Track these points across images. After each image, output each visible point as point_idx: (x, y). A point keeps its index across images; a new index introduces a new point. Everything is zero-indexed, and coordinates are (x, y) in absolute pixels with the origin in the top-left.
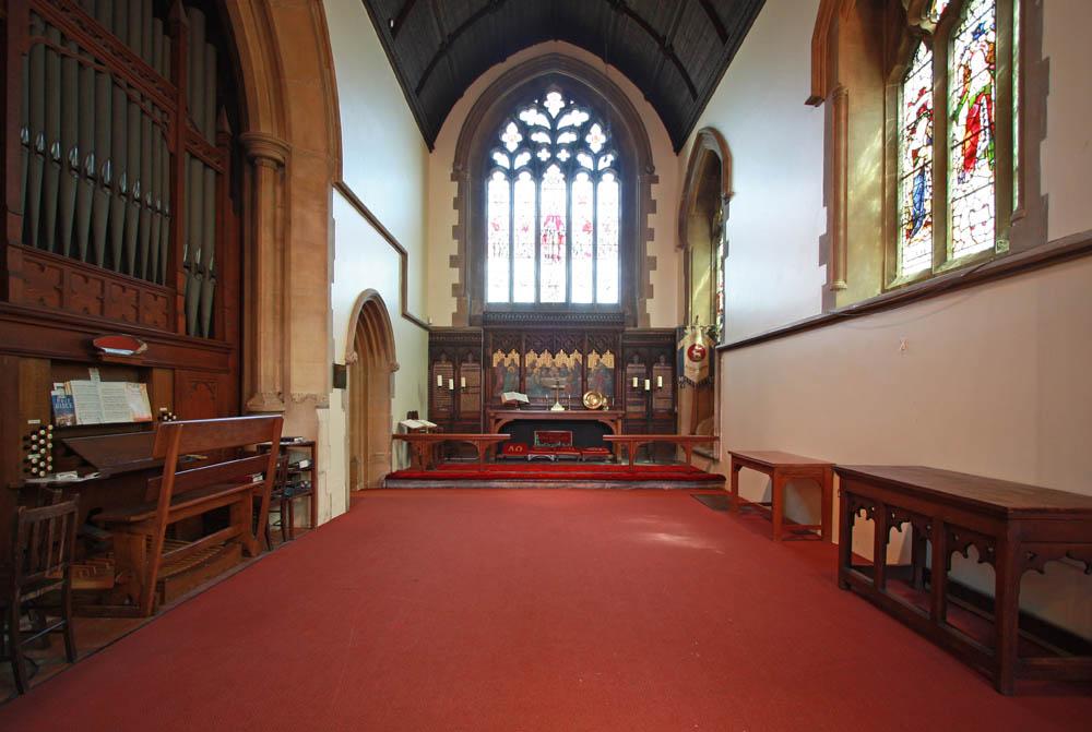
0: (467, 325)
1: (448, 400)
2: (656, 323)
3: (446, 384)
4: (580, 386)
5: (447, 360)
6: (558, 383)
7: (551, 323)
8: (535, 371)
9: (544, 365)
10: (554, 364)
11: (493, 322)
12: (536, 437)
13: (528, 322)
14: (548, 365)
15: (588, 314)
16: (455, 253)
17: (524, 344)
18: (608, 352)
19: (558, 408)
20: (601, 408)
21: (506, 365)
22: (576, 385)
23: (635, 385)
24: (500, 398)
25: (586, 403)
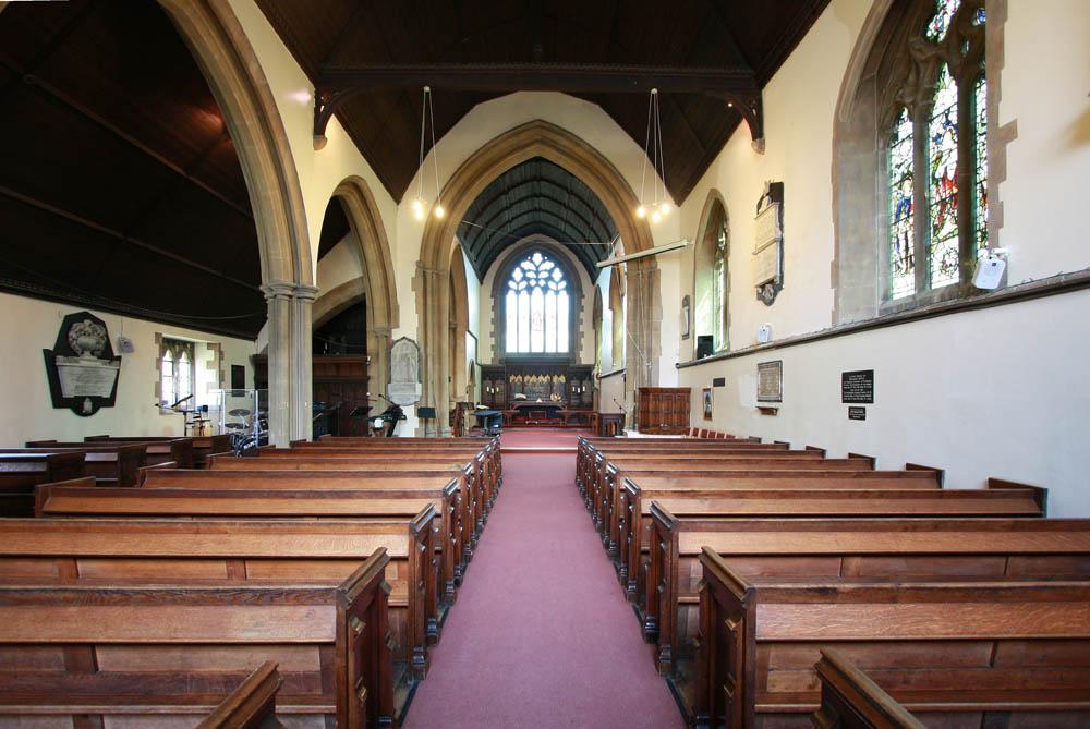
19: (539, 401)
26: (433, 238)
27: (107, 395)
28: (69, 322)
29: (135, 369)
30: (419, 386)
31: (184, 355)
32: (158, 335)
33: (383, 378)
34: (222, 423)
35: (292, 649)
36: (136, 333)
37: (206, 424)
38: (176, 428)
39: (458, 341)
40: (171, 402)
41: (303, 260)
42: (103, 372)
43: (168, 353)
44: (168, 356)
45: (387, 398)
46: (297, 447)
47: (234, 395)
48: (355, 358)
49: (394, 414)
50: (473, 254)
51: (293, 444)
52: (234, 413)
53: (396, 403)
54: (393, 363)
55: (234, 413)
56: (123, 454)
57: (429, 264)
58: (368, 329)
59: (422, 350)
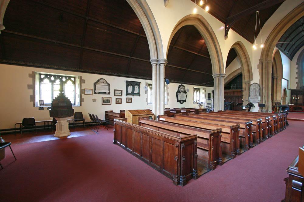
1: (295, 101)
2: (48, 100)
3: (295, 98)
16: (297, 86)
26: (265, 53)
27: (185, 100)
28: (180, 86)
29: (190, 94)
30: (259, 98)
31: (198, 91)
32: (193, 88)
33: (247, 95)
34: (205, 106)
36: (189, 87)
37: (202, 106)
38: (196, 107)
39: (278, 82)
40: (196, 101)
41: (222, 68)
42: (184, 95)
43: (195, 91)
44: (195, 91)
45: (248, 101)
46: (219, 112)
47: (208, 100)
48: (239, 90)
49: (251, 105)
50: (286, 52)
51: (218, 111)
52: (208, 104)
53: (251, 102)
54: (251, 91)
55: (208, 104)
56: (187, 111)
57: (264, 60)
58: (243, 82)
59: (261, 86)
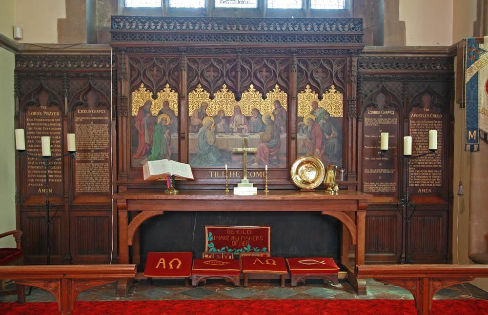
0: (85, 42)
4: (284, 149)
5: (50, 104)
6: (246, 144)
7: (234, 36)
8: (205, 121)
9: (221, 111)
10: (238, 110)
11: (133, 35)
12: (209, 237)
13: (192, 36)
14: (229, 112)
15: (298, 20)
17: (185, 74)
18: (333, 90)
19: (245, 190)
20: (323, 187)
21: (155, 112)
22: (278, 146)
23: (385, 146)
24: (141, 170)
25: (297, 179)
35: (218, 201)
